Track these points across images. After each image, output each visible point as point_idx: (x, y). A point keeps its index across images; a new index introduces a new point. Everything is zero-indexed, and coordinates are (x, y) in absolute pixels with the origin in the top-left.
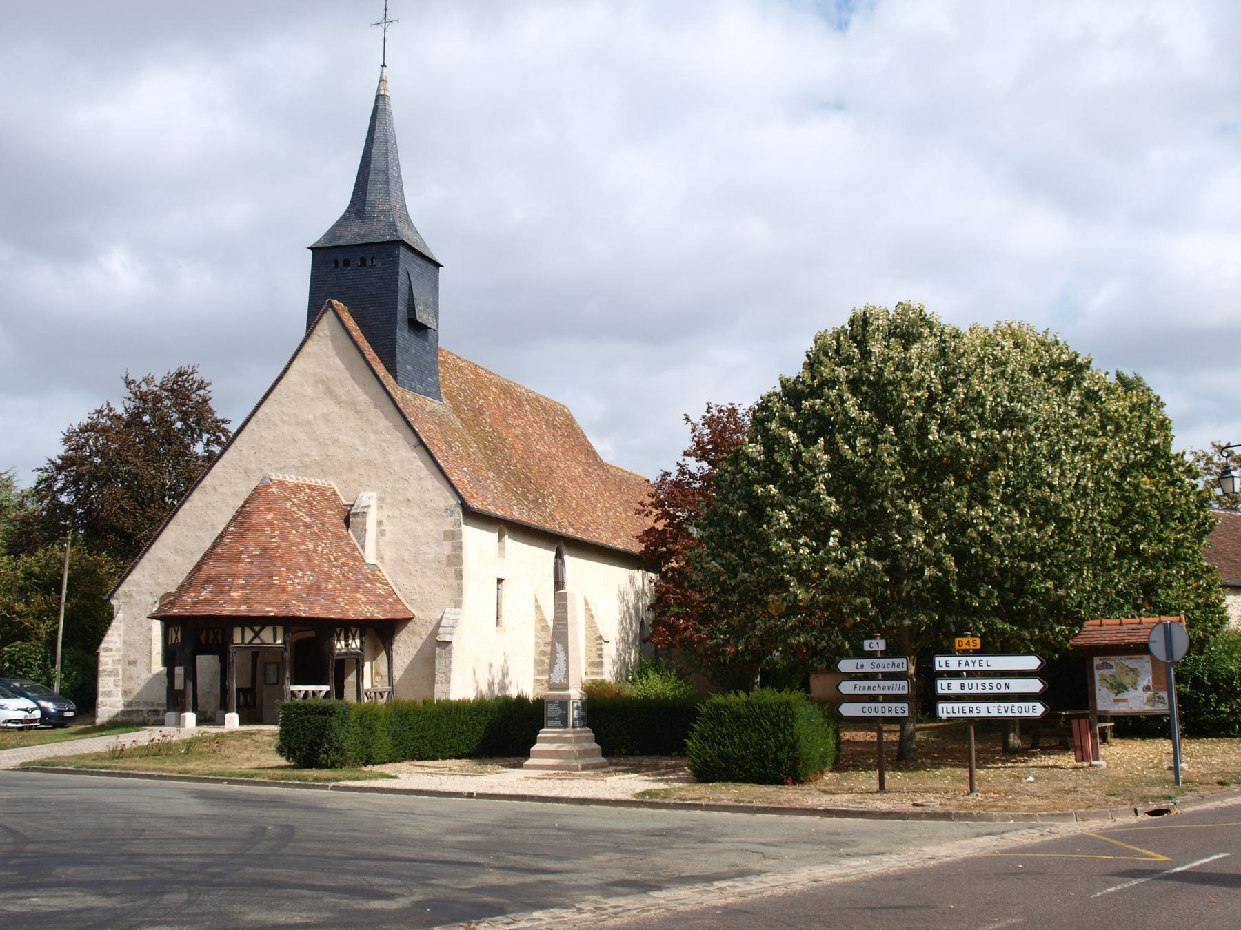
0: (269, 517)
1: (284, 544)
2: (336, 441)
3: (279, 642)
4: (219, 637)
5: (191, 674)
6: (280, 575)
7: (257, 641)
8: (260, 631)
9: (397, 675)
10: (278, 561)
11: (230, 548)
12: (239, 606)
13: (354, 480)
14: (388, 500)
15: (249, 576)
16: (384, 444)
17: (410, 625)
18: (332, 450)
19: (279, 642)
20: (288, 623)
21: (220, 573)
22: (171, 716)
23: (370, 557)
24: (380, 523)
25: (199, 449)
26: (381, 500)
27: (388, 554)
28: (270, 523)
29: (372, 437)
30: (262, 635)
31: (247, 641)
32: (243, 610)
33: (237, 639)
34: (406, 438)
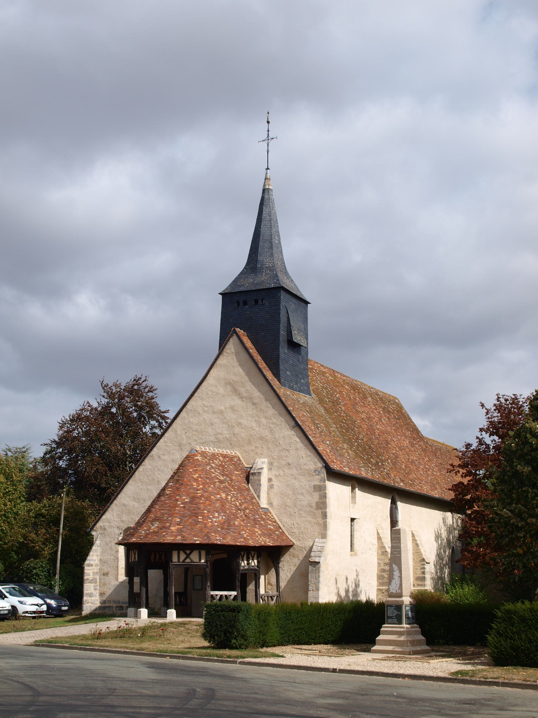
0: (195, 476)
1: (206, 494)
2: (239, 424)
5: (145, 583)
7: (188, 560)
8: (190, 553)
9: (283, 584)
10: (202, 506)
11: (170, 497)
12: (176, 536)
14: (276, 464)
15: (182, 516)
16: (272, 426)
17: (291, 550)
18: (237, 430)
19: (203, 561)
20: (209, 548)
21: (163, 514)
22: (131, 610)
23: (264, 503)
24: (270, 480)
26: (271, 464)
27: (276, 502)
28: (196, 480)
29: (264, 421)
31: (181, 560)
32: (179, 539)
33: (175, 559)
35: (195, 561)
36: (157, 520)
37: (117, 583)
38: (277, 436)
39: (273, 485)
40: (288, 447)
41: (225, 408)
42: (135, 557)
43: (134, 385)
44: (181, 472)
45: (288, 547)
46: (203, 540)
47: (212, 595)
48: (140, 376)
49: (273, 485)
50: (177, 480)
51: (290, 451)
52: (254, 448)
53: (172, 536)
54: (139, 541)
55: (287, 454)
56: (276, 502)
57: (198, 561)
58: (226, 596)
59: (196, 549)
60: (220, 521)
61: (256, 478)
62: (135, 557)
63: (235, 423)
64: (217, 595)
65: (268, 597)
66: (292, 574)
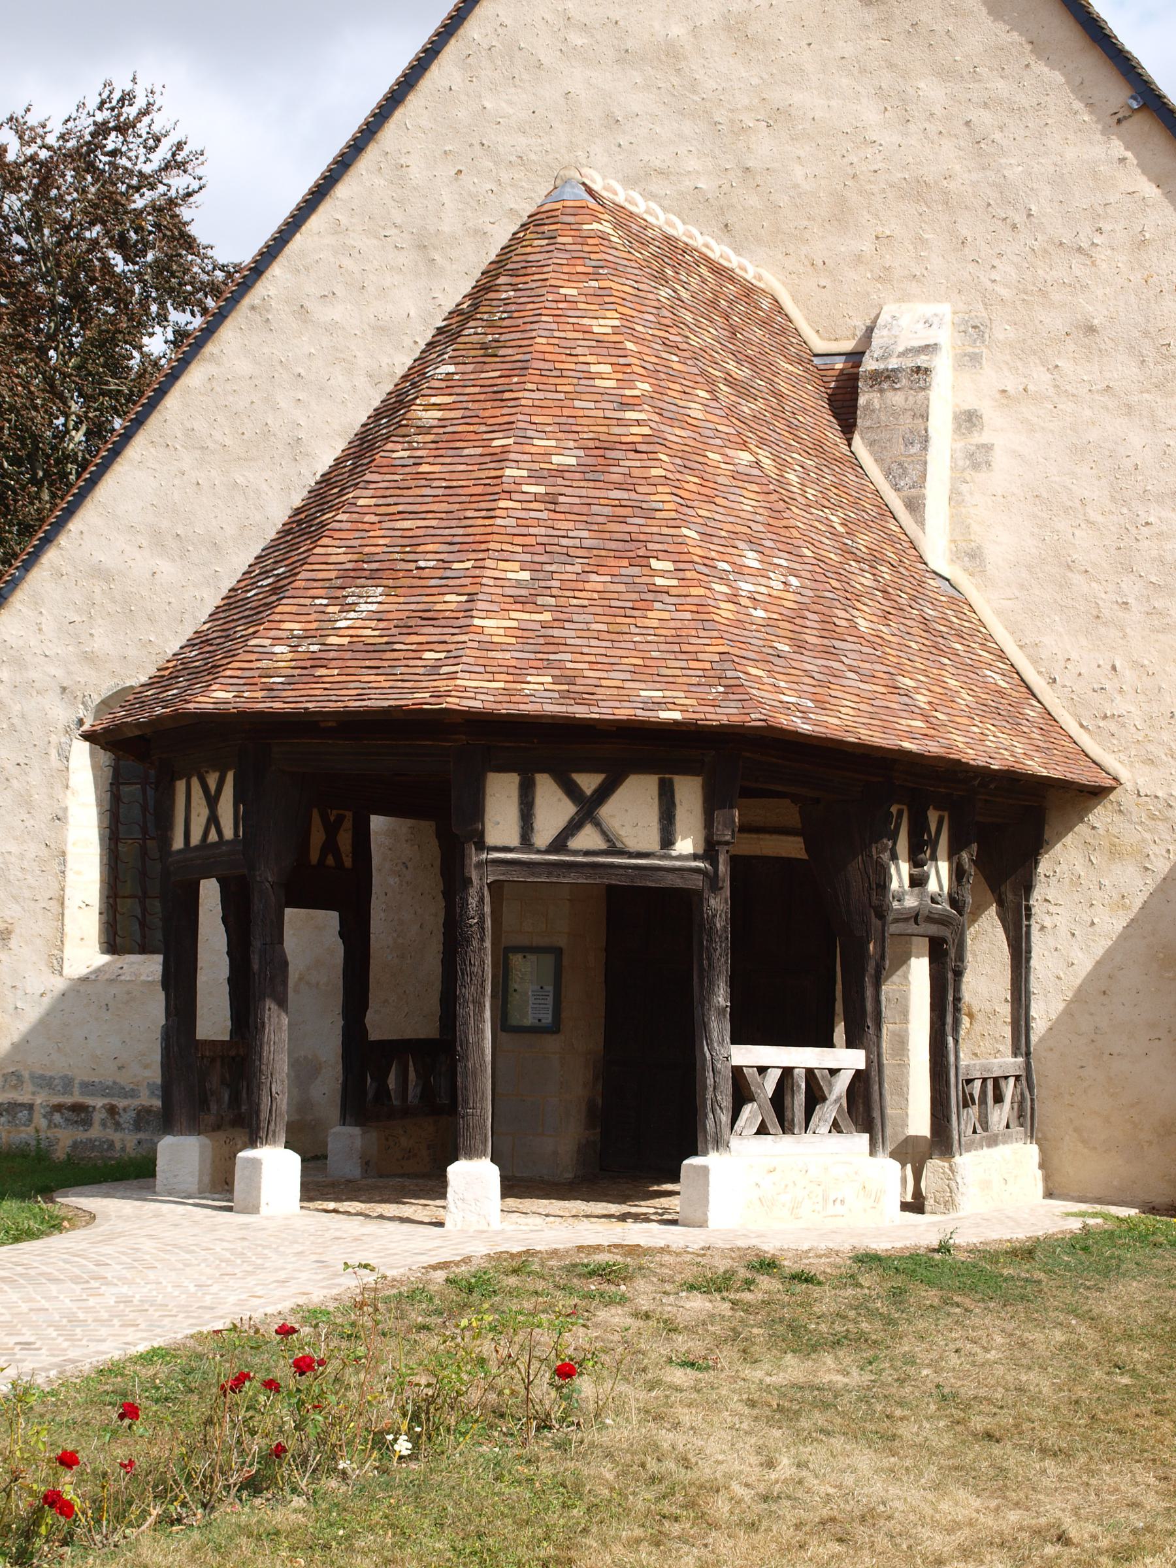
0: (602, 326)
1: (675, 434)
2: (779, 117)
3: (685, 846)
4: (317, 837)
6: (682, 560)
7: (587, 839)
8: (604, 793)
9: (1044, 1012)
10: (662, 498)
11: (446, 441)
12: (517, 673)
13: (858, 259)
14: (1002, 331)
15: (543, 553)
16: (984, 119)
17: (1100, 816)
18: (764, 148)
19: (685, 846)
20: (736, 762)
21: (412, 543)
22: (182, 1153)
23: (937, 548)
24: (968, 420)
25: (156, 344)
26: (975, 330)
27: (1004, 543)
28: (606, 347)
29: (932, 91)
30: (609, 811)
31: (544, 835)
32: (539, 695)
33: (501, 825)
34: (1079, 88)
35: (633, 845)
36: (374, 575)
37: (59, 984)
38: (1014, 173)
39: (988, 448)
40: (1086, 230)
41: (695, 31)
42: (214, 819)
43: (102, 130)
44: (507, 302)
45: (1084, 795)
46: (702, 702)
47: (737, 1071)
48: (128, 87)
49: (988, 448)
50: (484, 347)
51: (1101, 255)
52: (867, 246)
53: (489, 671)
54: (256, 700)
55: (1078, 270)
56: (1004, 543)
57: (653, 845)
58: (810, 1072)
59: (643, 767)
60: (773, 601)
61: (897, 399)
62: (214, 819)
63: (749, 109)
64: (762, 1070)
65: (985, 1080)
66: (1100, 947)
